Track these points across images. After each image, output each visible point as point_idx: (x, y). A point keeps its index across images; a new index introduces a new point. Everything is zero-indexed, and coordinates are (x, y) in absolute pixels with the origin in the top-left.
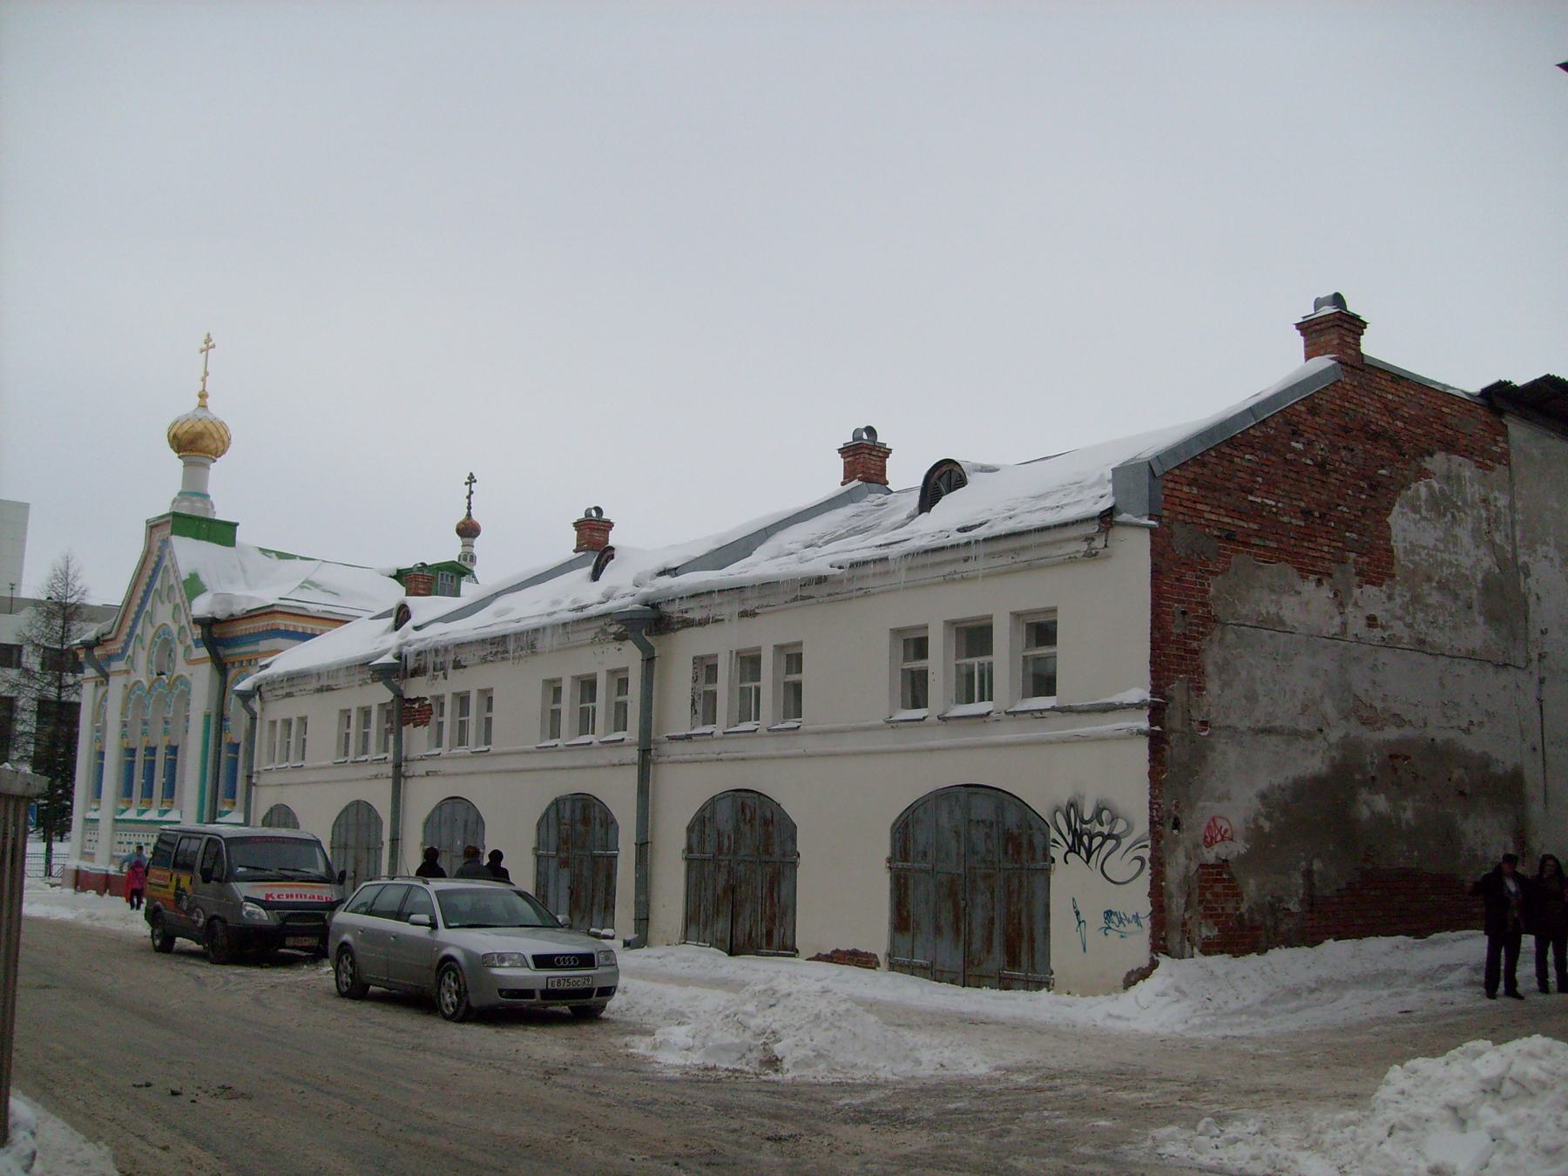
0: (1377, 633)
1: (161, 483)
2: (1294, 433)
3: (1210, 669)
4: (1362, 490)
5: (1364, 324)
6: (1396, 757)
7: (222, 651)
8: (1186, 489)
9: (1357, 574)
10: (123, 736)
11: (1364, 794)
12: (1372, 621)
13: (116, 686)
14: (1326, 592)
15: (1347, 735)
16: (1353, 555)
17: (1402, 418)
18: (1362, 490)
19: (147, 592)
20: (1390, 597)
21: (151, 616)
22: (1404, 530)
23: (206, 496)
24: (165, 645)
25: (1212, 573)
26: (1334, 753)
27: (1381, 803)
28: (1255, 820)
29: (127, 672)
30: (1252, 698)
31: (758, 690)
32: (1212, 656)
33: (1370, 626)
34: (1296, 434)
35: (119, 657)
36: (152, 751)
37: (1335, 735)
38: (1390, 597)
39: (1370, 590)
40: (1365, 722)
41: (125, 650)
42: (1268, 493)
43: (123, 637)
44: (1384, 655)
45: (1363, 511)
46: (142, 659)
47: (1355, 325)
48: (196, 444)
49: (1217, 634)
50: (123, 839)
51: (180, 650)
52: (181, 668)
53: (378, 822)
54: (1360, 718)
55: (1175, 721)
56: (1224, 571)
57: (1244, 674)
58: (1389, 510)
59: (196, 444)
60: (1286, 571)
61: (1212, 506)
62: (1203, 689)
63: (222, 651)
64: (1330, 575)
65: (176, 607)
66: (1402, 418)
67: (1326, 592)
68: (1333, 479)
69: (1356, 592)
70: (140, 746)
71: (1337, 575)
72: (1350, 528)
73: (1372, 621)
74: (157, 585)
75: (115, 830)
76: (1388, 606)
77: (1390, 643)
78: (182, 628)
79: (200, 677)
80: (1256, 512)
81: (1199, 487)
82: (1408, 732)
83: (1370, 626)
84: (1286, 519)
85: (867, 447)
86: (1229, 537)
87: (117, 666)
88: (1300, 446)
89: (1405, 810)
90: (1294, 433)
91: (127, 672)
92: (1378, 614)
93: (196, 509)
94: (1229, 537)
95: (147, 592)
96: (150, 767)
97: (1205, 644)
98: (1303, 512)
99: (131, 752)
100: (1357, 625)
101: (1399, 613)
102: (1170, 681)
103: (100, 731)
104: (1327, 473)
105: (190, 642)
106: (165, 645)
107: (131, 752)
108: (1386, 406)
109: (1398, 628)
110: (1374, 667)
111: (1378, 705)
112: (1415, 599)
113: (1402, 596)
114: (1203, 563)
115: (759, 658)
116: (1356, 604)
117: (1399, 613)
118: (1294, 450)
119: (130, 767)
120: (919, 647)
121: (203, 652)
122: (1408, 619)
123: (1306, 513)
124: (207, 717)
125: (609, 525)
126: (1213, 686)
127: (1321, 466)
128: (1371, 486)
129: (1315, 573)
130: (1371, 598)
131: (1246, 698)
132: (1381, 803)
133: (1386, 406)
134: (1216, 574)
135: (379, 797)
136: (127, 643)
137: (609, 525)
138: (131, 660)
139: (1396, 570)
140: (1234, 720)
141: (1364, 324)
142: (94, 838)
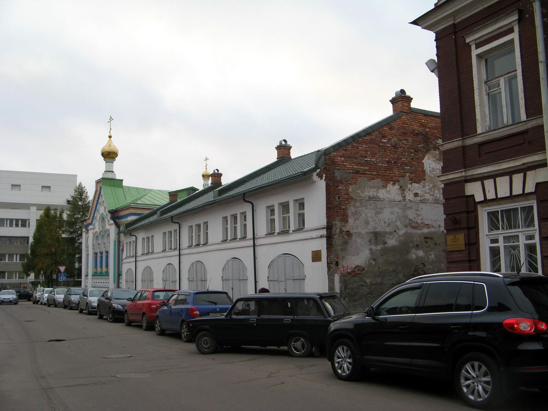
0: (419, 198)
1: (99, 168)
2: (383, 137)
3: (350, 214)
4: (412, 153)
5: (412, 99)
6: (427, 238)
7: (118, 221)
8: (339, 159)
9: (410, 180)
10: (93, 249)
11: (413, 251)
12: (416, 195)
13: (91, 233)
14: (397, 187)
15: (406, 232)
16: (408, 174)
17: (428, 128)
18: (412, 153)
19: (97, 204)
20: (424, 187)
21: (98, 210)
22: (429, 164)
23: (113, 172)
24: (103, 219)
25: (350, 184)
26: (401, 238)
27: (421, 253)
28: (369, 261)
29: (93, 229)
30: (367, 223)
31: (289, 217)
32: (351, 210)
33: (415, 196)
34: (384, 137)
35: (91, 224)
36: (101, 253)
37: (401, 232)
38: (424, 187)
39: (415, 185)
40: (414, 228)
41: (92, 221)
42: (373, 157)
43: (91, 218)
44: (421, 206)
45: (412, 159)
46: (97, 224)
47: (409, 99)
48: (109, 156)
49: (352, 203)
50: (95, 281)
51: (107, 220)
52: (107, 227)
53: (244, 268)
54: (412, 226)
55: (336, 230)
56: (355, 183)
57: (363, 215)
58: (423, 158)
59: (109, 156)
60: (377, 182)
61: (350, 163)
62: (347, 221)
63: (118, 221)
64: (398, 181)
65: (105, 207)
66: (428, 128)
67: (397, 187)
68: (400, 150)
69: (410, 186)
70: (98, 251)
71: (401, 181)
72: (407, 165)
73: (416, 195)
74: (100, 201)
75: (93, 278)
76: (423, 189)
77: (424, 201)
78: (107, 214)
79: (112, 229)
80: (367, 163)
81: (345, 158)
82: (432, 230)
83: (415, 196)
84: (380, 165)
85: (285, 146)
86: (357, 172)
87: (91, 227)
88: (386, 141)
89: (431, 255)
90: (383, 137)
91: (93, 229)
92: (419, 192)
93: (109, 176)
94: (357, 172)
95: (97, 204)
96: (102, 257)
97: (348, 206)
98: (387, 162)
99: (96, 254)
100: (410, 196)
101: (428, 191)
102: (334, 220)
103: (87, 247)
104: (397, 148)
105: (109, 218)
106: (103, 219)
107: (96, 254)
108: (421, 124)
109: (427, 196)
110: (417, 210)
111: (419, 222)
112: (434, 186)
113: (428, 185)
114: (347, 181)
115: (289, 205)
116: (409, 190)
117: (428, 191)
118: (383, 142)
119: (96, 258)
120: (272, 212)
121: (112, 222)
122: (432, 193)
123: (389, 162)
124: (115, 241)
125: (221, 175)
126: (351, 220)
127: (395, 147)
128: (415, 151)
129: (392, 181)
130: (416, 187)
131: (365, 223)
132: (421, 253)
133: (421, 124)
134: (352, 184)
135: (246, 256)
136: (93, 220)
137: (221, 175)
138: (94, 225)
139: (426, 177)
140: (359, 230)
141: (412, 99)
142: (108, 281)
